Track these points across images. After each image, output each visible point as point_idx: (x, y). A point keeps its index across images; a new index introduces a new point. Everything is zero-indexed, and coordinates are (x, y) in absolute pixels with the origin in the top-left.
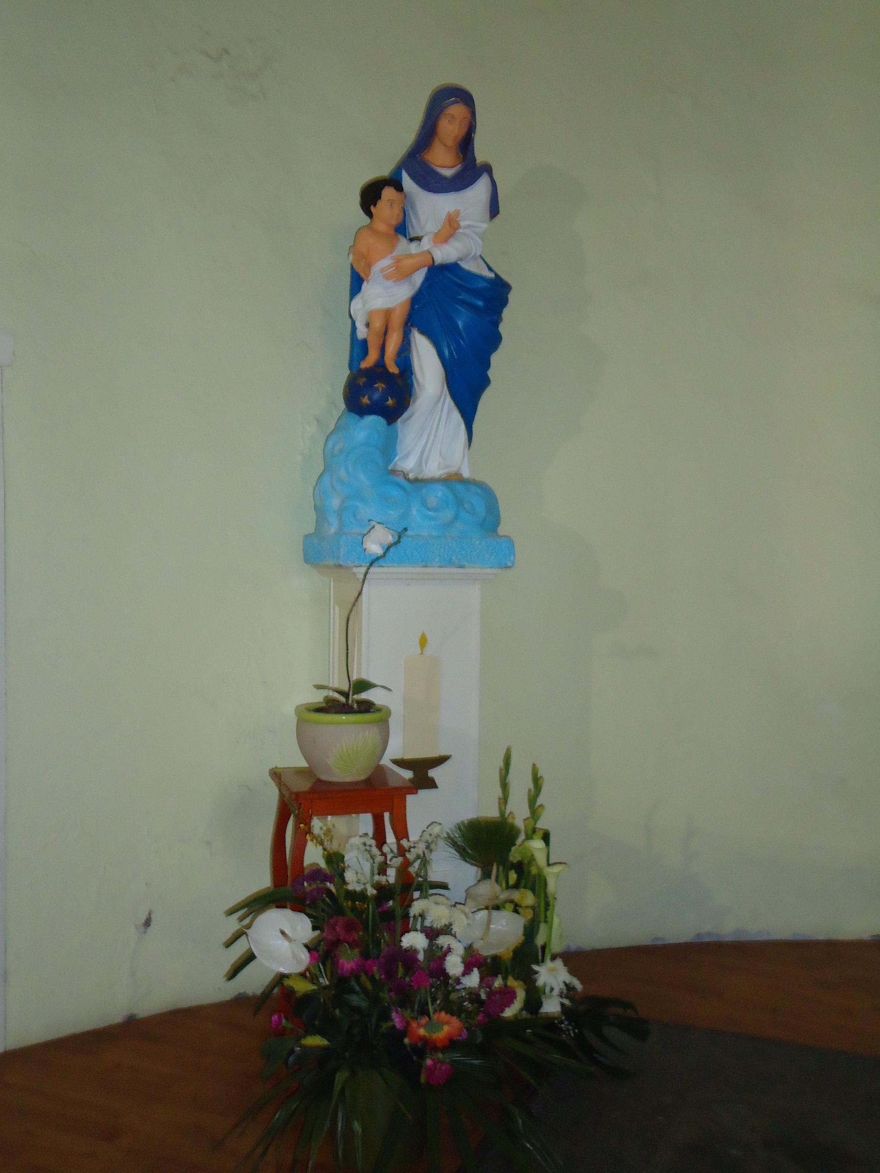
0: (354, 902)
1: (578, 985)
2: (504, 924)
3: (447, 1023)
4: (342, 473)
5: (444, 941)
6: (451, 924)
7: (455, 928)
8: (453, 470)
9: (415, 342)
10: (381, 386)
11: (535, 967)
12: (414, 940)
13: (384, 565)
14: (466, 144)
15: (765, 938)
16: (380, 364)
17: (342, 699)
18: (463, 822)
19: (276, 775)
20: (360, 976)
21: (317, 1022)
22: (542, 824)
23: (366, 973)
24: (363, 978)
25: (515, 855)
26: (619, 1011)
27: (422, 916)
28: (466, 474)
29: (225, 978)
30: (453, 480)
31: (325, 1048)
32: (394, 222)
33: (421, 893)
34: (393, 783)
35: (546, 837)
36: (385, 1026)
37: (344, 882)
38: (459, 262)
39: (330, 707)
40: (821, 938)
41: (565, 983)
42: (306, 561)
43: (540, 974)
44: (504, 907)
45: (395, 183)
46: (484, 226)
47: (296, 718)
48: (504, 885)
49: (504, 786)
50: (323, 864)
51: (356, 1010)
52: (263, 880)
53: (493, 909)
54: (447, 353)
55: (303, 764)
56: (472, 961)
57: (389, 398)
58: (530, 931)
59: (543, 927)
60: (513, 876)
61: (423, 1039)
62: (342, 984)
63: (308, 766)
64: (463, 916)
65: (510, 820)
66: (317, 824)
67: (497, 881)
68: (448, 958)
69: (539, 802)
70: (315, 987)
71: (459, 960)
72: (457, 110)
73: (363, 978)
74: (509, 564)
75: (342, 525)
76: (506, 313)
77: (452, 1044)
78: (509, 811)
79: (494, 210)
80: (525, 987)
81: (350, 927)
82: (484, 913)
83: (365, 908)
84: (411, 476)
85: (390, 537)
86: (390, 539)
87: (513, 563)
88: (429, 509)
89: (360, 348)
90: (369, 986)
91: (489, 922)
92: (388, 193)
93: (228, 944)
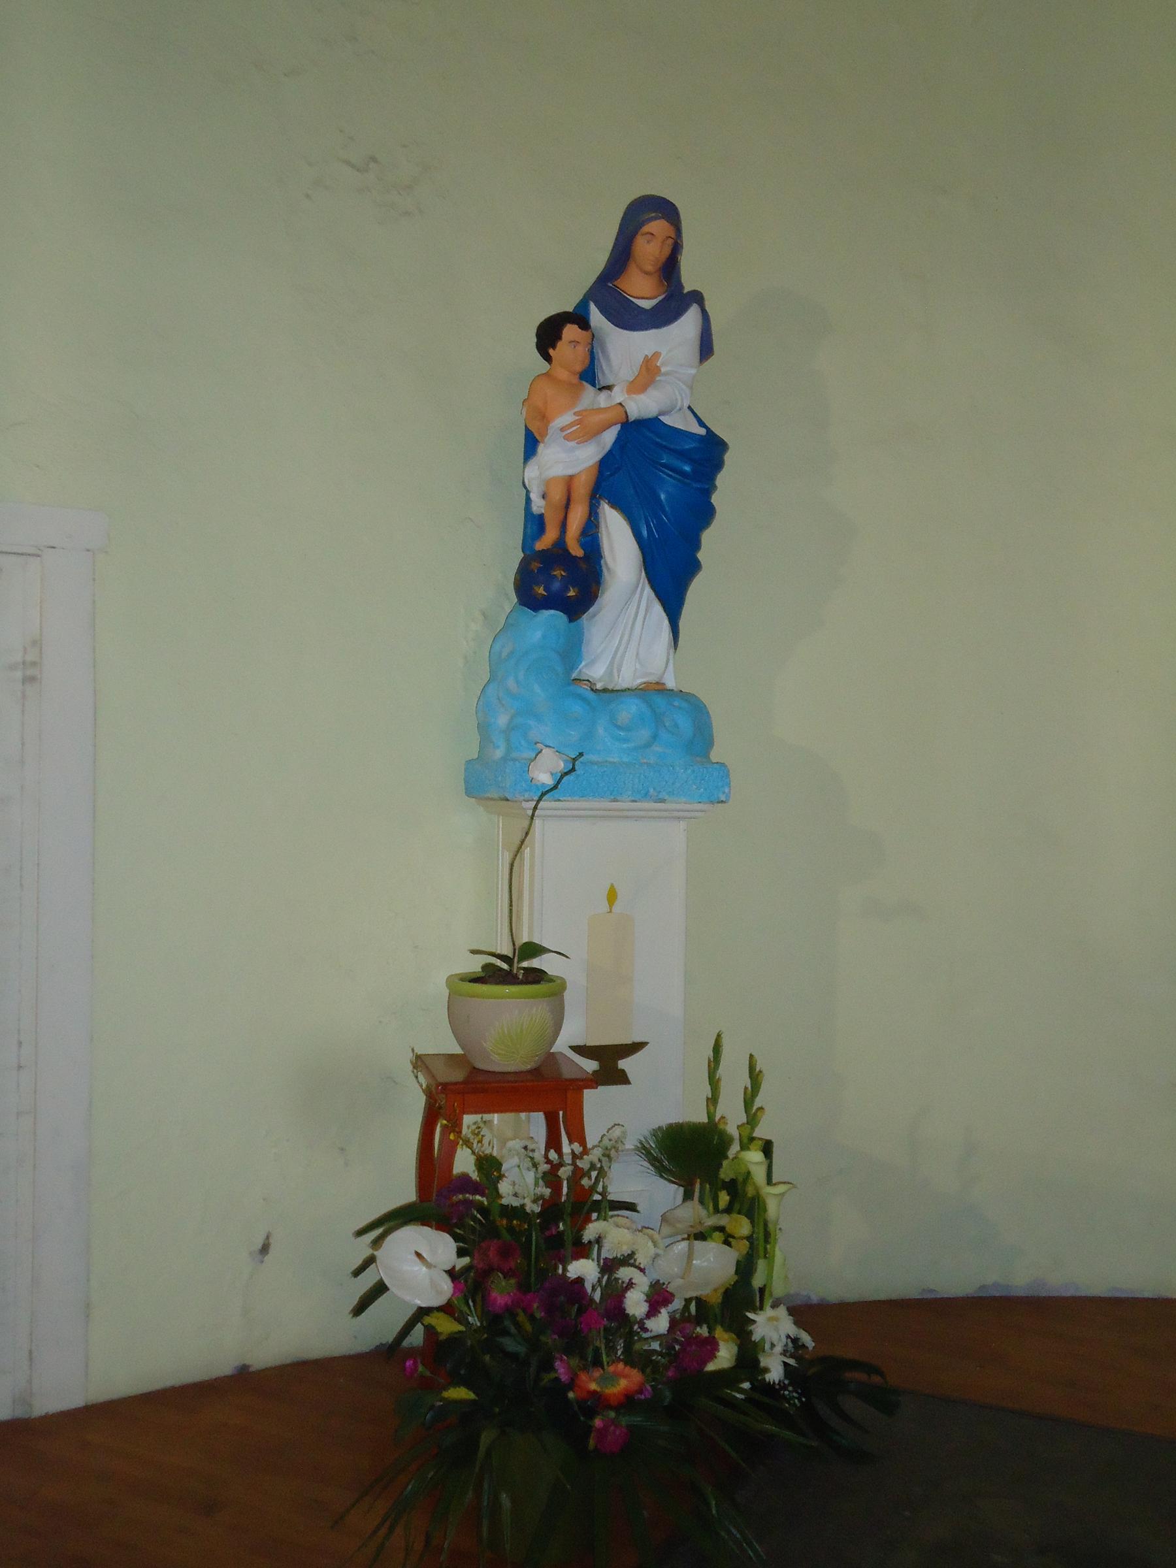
0: (510, 1220)
1: (806, 1339)
2: (712, 1259)
3: (625, 1377)
4: (511, 683)
5: (624, 1273)
6: (633, 1253)
7: (641, 1259)
8: (652, 679)
9: (605, 518)
10: (558, 573)
11: (751, 1315)
12: (584, 1269)
13: (561, 799)
14: (669, 268)
15: (1070, 1293)
16: (560, 543)
17: (505, 966)
18: (660, 1128)
19: (420, 1062)
20: (517, 1315)
21: (462, 1372)
22: (761, 1132)
23: (524, 1310)
24: (522, 1317)
25: (726, 1172)
26: (861, 1376)
27: (599, 1240)
28: (671, 683)
29: (351, 1315)
30: (653, 690)
31: (473, 1402)
32: (579, 368)
33: (598, 1215)
34: (567, 1073)
35: (768, 1149)
36: (547, 1377)
37: (500, 1196)
38: (661, 418)
39: (490, 976)
40: (1147, 1295)
41: (788, 1337)
42: (469, 793)
43: (757, 1324)
44: (711, 1237)
45: (579, 318)
46: (693, 371)
47: (448, 991)
48: (711, 1208)
49: (714, 1082)
50: (475, 1176)
51: (514, 1357)
52: (406, 1192)
53: (696, 1239)
54: (645, 533)
55: (458, 1051)
56: (658, 1297)
57: (545, 594)
58: (745, 1269)
59: (761, 1264)
60: (724, 1198)
61: (594, 1393)
62: (495, 1322)
63: (463, 1053)
64: (650, 1244)
65: (721, 1126)
66: (468, 1120)
67: (701, 1202)
68: (629, 1294)
69: (758, 1102)
70: (462, 1328)
71: (643, 1297)
72: (658, 227)
73: (522, 1317)
74: (723, 798)
75: (509, 749)
76: (722, 479)
77: (628, 1402)
78: (720, 1116)
79: (706, 348)
80: (739, 1342)
81: (506, 1252)
82: (684, 1244)
83: (525, 1229)
84: (599, 686)
85: (562, 765)
86: (561, 766)
87: (728, 796)
88: (619, 728)
89: (535, 524)
90: (528, 1327)
91: (690, 1256)
92: (570, 332)
93: (357, 1273)
